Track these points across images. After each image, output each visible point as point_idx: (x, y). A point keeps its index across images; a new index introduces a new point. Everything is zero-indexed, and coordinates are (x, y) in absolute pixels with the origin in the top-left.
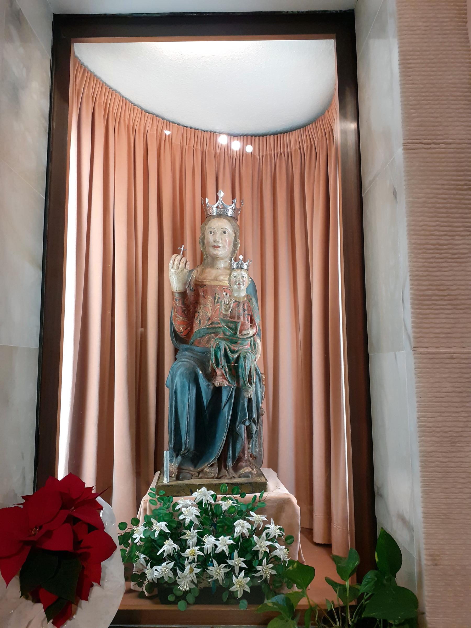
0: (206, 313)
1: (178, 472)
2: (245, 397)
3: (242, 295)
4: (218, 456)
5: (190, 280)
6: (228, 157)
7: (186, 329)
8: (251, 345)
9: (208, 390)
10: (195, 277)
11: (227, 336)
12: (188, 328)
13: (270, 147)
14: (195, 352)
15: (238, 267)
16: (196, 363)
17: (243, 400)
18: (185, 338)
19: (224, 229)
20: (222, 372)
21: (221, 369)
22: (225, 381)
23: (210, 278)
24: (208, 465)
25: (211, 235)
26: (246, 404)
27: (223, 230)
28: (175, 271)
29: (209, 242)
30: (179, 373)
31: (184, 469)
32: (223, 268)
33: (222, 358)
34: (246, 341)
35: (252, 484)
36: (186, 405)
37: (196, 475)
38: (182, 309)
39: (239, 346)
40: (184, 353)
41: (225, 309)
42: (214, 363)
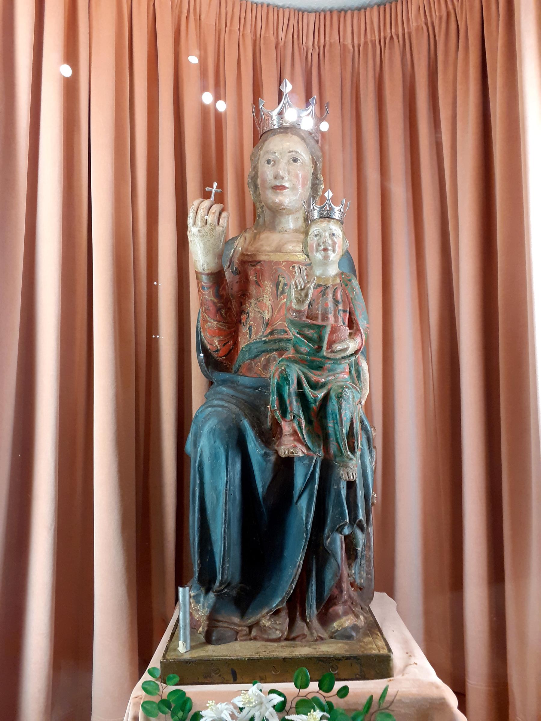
0: (261, 313)
1: (209, 626)
2: (340, 478)
3: (331, 272)
4: (287, 596)
5: (233, 255)
6: (299, 48)
7: (225, 344)
8: (350, 372)
9: (265, 463)
10: (240, 248)
11: (302, 353)
12: (228, 342)
13: (372, 29)
14: (240, 388)
15: (322, 217)
16: (240, 409)
17: (338, 484)
18: (224, 361)
19: (294, 153)
20: (293, 427)
21: (291, 420)
22: (299, 446)
23: (268, 249)
24: (267, 613)
25: (270, 165)
26: (344, 492)
27: (291, 155)
28: (199, 231)
29: (266, 181)
30: (206, 429)
31: (219, 621)
32: (293, 230)
33: (292, 399)
34: (340, 364)
35: (359, 659)
36: (221, 494)
37: (245, 633)
38: (216, 306)
39: (326, 373)
40: (218, 389)
41: (296, 298)
42: (276, 408)
